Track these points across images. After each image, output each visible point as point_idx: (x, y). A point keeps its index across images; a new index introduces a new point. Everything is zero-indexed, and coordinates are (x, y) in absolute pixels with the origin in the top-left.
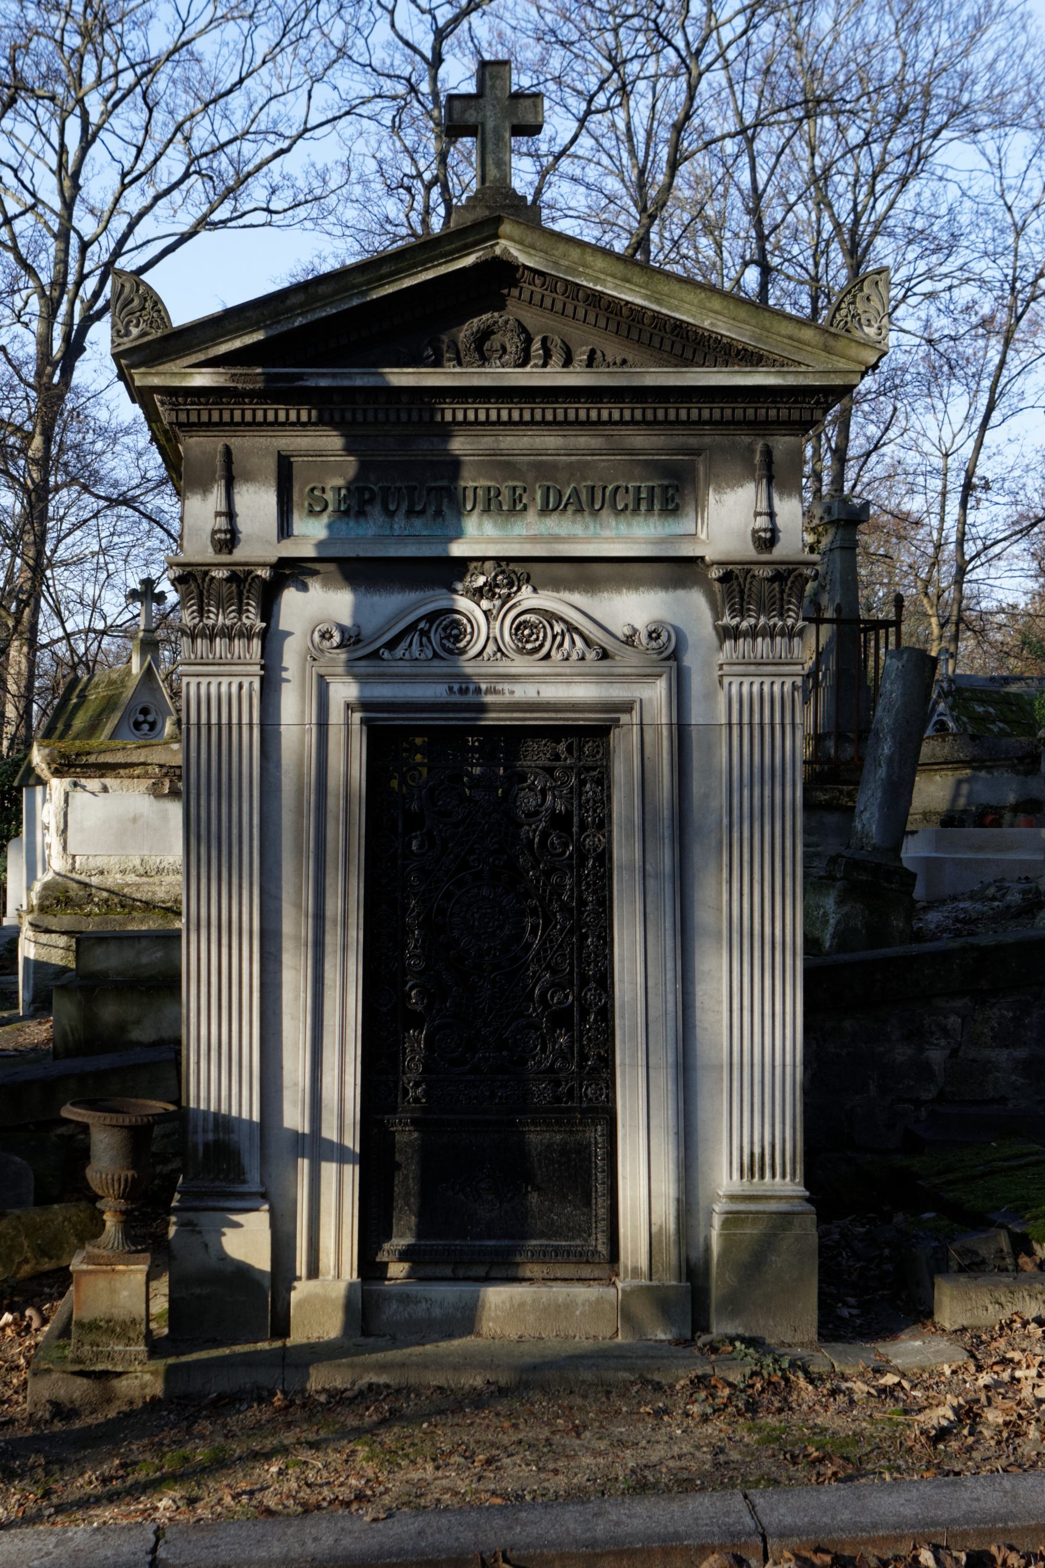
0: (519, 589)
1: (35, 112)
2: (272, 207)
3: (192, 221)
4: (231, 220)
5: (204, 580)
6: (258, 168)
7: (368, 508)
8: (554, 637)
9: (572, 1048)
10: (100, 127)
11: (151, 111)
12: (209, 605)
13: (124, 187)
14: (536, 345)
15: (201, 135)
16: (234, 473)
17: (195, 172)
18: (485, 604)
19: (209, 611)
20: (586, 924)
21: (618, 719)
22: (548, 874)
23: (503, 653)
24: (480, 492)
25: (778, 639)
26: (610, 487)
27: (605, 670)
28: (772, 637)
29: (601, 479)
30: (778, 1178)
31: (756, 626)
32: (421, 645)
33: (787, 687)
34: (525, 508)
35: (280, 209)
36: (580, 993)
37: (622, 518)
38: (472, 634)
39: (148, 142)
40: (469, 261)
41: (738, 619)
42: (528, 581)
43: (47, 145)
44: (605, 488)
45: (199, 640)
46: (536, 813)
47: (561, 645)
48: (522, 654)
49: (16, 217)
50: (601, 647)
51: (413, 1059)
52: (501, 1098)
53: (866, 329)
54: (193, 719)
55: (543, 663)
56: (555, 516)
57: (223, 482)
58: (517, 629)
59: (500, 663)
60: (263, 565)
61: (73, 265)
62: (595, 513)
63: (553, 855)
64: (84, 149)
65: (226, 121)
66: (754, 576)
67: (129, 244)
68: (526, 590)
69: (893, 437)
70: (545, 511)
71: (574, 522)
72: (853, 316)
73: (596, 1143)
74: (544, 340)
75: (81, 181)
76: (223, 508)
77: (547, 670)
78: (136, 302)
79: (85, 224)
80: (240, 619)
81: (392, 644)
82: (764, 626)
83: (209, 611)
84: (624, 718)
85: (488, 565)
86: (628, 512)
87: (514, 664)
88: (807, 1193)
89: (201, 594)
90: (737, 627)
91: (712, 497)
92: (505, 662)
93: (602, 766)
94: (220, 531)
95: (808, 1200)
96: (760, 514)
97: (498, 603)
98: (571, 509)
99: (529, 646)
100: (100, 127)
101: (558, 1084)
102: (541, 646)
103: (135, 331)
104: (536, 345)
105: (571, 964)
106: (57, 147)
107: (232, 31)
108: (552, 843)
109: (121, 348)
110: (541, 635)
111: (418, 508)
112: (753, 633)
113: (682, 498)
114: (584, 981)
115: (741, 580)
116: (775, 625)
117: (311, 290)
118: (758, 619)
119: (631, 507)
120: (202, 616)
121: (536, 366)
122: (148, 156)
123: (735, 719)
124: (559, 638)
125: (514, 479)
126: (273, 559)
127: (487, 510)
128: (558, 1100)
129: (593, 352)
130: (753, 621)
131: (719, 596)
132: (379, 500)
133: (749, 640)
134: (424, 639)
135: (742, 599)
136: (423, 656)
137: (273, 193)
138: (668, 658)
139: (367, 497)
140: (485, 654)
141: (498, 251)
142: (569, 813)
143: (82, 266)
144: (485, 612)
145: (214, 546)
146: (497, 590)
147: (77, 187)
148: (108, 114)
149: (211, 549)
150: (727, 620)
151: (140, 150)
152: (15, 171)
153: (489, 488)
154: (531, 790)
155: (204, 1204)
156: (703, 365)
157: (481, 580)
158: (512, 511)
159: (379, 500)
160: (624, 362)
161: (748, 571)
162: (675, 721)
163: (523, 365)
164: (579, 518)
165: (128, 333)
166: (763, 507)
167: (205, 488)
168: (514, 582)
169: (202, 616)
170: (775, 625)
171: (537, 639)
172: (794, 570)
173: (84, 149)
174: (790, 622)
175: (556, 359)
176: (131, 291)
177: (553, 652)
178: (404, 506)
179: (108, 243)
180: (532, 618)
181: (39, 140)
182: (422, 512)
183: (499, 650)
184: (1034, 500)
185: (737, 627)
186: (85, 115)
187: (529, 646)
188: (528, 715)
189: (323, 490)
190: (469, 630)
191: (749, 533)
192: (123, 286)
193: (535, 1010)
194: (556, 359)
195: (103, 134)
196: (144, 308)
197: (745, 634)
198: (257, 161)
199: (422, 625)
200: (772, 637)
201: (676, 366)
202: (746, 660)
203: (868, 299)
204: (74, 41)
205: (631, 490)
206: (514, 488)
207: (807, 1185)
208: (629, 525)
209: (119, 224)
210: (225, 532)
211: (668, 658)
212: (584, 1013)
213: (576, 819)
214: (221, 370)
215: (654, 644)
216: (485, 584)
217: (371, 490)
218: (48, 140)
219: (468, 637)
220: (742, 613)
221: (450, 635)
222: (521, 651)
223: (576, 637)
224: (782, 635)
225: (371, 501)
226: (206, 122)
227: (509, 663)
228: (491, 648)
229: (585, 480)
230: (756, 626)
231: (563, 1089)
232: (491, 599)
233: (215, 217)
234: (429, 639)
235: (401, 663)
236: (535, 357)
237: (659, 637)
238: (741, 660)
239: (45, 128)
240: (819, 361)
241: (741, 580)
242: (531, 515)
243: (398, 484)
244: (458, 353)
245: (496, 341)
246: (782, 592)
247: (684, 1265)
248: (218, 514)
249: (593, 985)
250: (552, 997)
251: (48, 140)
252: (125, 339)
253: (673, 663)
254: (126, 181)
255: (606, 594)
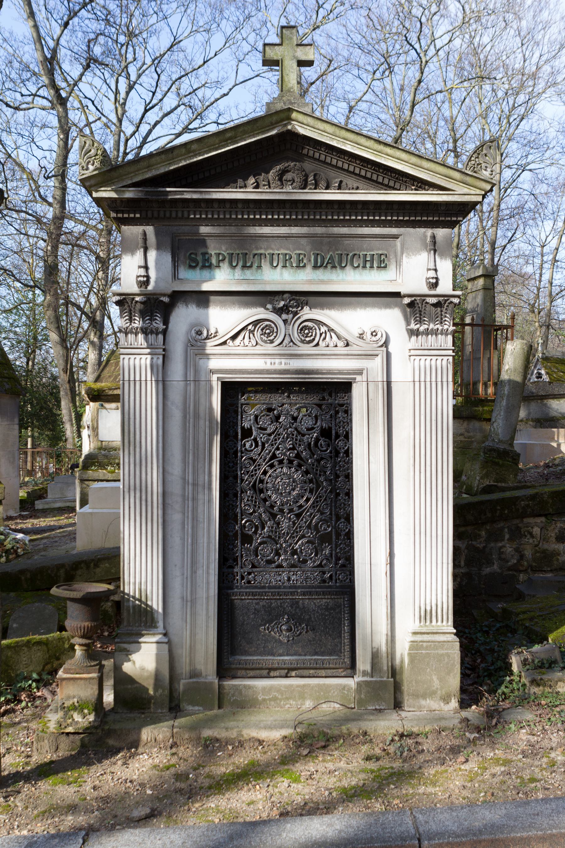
0: (302, 308)
1: (103, 74)
2: (219, 121)
3: (181, 129)
4: (199, 128)
5: (132, 303)
6: (212, 104)
7: (221, 264)
8: (321, 334)
9: (331, 554)
10: (135, 83)
11: (159, 76)
12: (135, 316)
13: (146, 111)
14: (311, 178)
15: (185, 86)
16: (148, 245)
17: (183, 104)
18: (284, 316)
19: (135, 319)
20: (339, 488)
21: (355, 379)
22: (318, 461)
23: (294, 343)
24: (281, 256)
25: (440, 336)
26: (351, 254)
27: (346, 352)
28: (436, 335)
29: (346, 250)
30: (439, 623)
31: (428, 329)
32: (250, 338)
33: (444, 362)
34: (304, 266)
35: (223, 122)
36: (335, 524)
37: (357, 271)
38: (277, 332)
39: (158, 89)
40: (274, 132)
41: (418, 326)
42: (307, 304)
43: (109, 89)
44: (348, 255)
45: (129, 335)
46: (313, 428)
47: (325, 339)
48: (304, 343)
49: (93, 122)
50: (347, 340)
51: (247, 560)
52: (293, 581)
53: (484, 172)
54: (126, 378)
55: (315, 348)
56: (321, 270)
57: (142, 250)
58: (301, 330)
59: (291, 348)
60: (164, 295)
61: (122, 149)
62: (343, 268)
63: (321, 451)
64: (128, 93)
65: (197, 80)
66: (427, 303)
67: (150, 139)
68: (306, 309)
69: (518, 237)
70: (315, 267)
71: (331, 273)
72: (478, 164)
73: (344, 605)
74: (315, 175)
75: (127, 108)
76: (142, 264)
77: (317, 352)
78: (93, 151)
79: (128, 128)
80: (151, 324)
81: (234, 338)
82: (432, 329)
83: (135, 319)
84: (358, 378)
85: (286, 296)
86: (198, 268)
87: (300, 348)
88: (455, 631)
89: (130, 310)
90: (418, 330)
91: (405, 259)
92: (295, 348)
93: (347, 404)
94: (141, 276)
95: (455, 634)
96: (430, 270)
97: (291, 316)
98: (329, 266)
99: (308, 339)
100: (135, 83)
101: (324, 573)
102: (314, 339)
103: (91, 167)
104: (311, 178)
105: (331, 510)
106: (114, 90)
107: (200, 37)
108: (321, 445)
109: (84, 176)
110: (314, 333)
111: (248, 265)
112: (427, 333)
113: (389, 261)
114: (338, 518)
115: (420, 305)
116: (438, 329)
117: (188, 147)
118: (429, 325)
119: (361, 265)
120: (131, 322)
121: (311, 189)
122: (159, 96)
123: (417, 379)
124: (323, 335)
125: (300, 249)
126: (169, 291)
127: (284, 266)
128: (324, 581)
129: (341, 182)
130: (426, 326)
131: (408, 313)
132: (227, 260)
133: (424, 336)
134: (251, 335)
135: (421, 315)
136: (250, 344)
137: (220, 115)
138: (382, 346)
139: (221, 258)
140: (284, 343)
141: (289, 127)
142: (330, 428)
143: (126, 149)
144: (284, 321)
145: (138, 285)
146: (291, 309)
147: (124, 112)
148: (139, 76)
149: (136, 286)
150: (413, 326)
151: (154, 93)
152: (93, 102)
153: (286, 254)
154: (309, 416)
155: (131, 640)
156: (399, 190)
157: (282, 303)
158: (298, 267)
159: (227, 260)
160: (357, 188)
161: (424, 300)
162: (385, 379)
163: (304, 188)
164: (334, 271)
165: (87, 169)
166: (432, 266)
167: (132, 251)
168: (301, 305)
169: (131, 322)
170: (438, 329)
171: (312, 336)
172: (446, 301)
173: (128, 93)
174: (446, 327)
175: (323, 184)
176: (89, 145)
177: (320, 343)
178: (241, 264)
179: (139, 138)
180: (309, 324)
181: (105, 87)
182: (251, 267)
183: (292, 341)
184: (6, 401)
185: (418, 330)
186: (128, 77)
187: (308, 339)
188: (307, 376)
189: (196, 254)
190: (275, 330)
191: (425, 280)
192: (85, 142)
193: (312, 533)
194: (323, 184)
195: (137, 86)
196: (97, 155)
197: (422, 334)
198: (212, 100)
199: (250, 327)
200: (436, 335)
201: (386, 190)
202: (423, 348)
203: (486, 155)
204: (122, 39)
205: (361, 256)
206: (300, 254)
207: (455, 627)
208: (361, 274)
209: (144, 129)
210: (144, 276)
211: (382, 346)
212: (338, 535)
213: (333, 432)
214: (140, 189)
215: (374, 339)
216: (284, 305)
217: (223, 255)
218: (110, 87)
219: (275, 334)
220: (421, 322)
221: (265, 333)
222: (303, 342)
223: (333, 334)
224: (442, 334)
225: (223, 260)
226: (187, 81)
227: (297, 348)
228: (287, 340)
229: (337, 250)
230: (428, 329)
231: (327, 575)
232: (287, 313)
233: (191, 127)
234: (253, 334)
235: (238, 348)
236: (310, 184)
237: (376, 335)
238: (420, 348)
239: (108, 82)
240: (461, 189)
241: (420, 305)
242: (309, 269)
243: (237, 252)
244: (269, 182)
245: (289, 176)
246: (442, 311)
247: (390, 669)
248: (140, 267)
249: (343, 520)
250: (321, 527)
251: (110, 87)
252: (85, 172)
253: (384, 349)
254: (148, 108)
255: (358, 309)
